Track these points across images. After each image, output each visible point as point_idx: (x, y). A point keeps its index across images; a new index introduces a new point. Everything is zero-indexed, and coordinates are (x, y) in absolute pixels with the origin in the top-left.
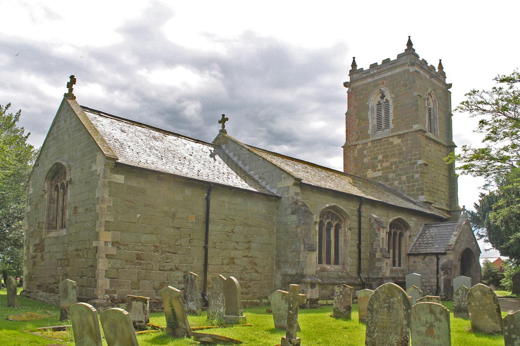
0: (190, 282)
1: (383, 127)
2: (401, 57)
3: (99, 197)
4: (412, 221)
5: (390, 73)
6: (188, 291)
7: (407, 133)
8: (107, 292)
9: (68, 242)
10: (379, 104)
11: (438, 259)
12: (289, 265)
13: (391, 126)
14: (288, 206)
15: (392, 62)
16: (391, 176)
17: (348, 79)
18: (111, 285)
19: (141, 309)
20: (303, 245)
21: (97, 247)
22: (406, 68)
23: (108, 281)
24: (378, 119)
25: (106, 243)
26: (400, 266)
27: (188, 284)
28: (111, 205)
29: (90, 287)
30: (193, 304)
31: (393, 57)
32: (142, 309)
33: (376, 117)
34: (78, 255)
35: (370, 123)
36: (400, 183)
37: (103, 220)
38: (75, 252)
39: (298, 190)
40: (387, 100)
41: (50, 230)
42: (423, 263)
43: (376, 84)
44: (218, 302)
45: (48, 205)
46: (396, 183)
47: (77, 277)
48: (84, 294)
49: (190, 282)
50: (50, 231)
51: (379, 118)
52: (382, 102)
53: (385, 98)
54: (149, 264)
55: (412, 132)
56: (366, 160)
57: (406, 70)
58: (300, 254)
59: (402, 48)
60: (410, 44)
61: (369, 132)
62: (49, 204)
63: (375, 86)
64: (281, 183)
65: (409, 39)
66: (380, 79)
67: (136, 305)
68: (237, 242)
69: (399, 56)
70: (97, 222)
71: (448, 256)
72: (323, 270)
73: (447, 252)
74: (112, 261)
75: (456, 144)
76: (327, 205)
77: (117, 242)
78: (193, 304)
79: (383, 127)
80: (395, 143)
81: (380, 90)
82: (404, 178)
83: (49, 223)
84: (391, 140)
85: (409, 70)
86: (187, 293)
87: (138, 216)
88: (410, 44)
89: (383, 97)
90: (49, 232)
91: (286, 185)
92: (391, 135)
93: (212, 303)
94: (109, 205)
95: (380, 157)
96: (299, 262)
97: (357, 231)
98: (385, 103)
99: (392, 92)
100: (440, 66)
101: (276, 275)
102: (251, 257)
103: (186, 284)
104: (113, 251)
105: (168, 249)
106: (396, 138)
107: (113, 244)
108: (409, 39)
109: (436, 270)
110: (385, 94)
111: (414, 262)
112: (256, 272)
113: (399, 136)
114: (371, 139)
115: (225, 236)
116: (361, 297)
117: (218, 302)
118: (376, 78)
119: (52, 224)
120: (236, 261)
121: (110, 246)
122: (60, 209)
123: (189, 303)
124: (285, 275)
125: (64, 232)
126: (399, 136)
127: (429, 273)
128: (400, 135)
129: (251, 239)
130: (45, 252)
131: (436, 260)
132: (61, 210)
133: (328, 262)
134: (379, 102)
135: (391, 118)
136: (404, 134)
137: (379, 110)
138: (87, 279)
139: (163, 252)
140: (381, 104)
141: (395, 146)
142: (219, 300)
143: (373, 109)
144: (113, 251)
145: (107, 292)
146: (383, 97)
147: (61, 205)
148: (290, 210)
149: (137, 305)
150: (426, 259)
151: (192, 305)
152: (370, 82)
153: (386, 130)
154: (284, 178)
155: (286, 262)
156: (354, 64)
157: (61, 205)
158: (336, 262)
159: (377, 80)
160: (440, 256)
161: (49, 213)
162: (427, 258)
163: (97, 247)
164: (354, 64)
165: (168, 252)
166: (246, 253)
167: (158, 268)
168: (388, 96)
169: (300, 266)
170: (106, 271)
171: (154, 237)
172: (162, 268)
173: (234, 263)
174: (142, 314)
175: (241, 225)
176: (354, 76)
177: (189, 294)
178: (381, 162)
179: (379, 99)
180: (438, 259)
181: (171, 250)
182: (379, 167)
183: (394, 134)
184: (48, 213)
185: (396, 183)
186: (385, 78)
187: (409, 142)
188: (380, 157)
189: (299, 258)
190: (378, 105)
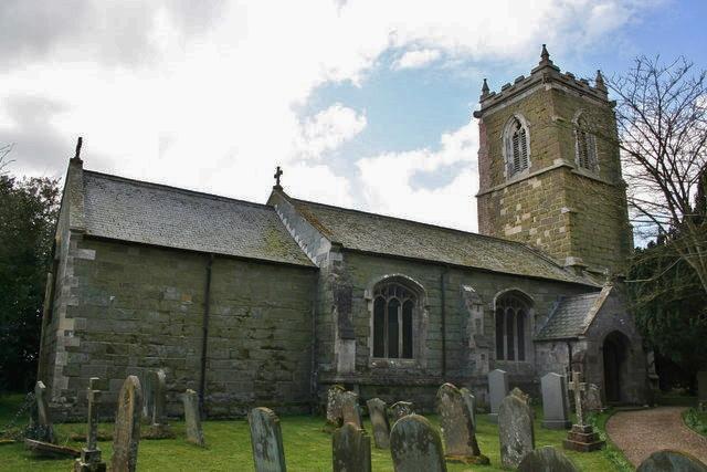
4: (538, 295)
8: (63, 394)
10: (516, 136)
13: (530, 164)
16: (533, 231)
17: (479, 107)
18: (70, 385)
22: (541, 86)
23: (66, 380)
25: (67, 333)
26: (522, 357)
28: (77, 285)
31: (527, 75)
36: (543, 241)
37: (64, 305)
39: (340, 257)
46: (539, 240)
48: (210, 387)
54: (124, 358)
56: (503, 212)
59: (536, 61)
60: (545, 54)
61: (505, 174)
68: (254, 329)
69: (534, 72)
72: (386, 366)
74: (74, 355)
76: (386, 276)
77: (82, 332)
80: (534, 187)
82: (547, 233)
84: (530, 182)
87: (112, 298)
88: (545, 54)
94: (73, 285)
95: (519, 207)
97: (439, 310)
99: (527, 119)
100: (600, 81)
102: (276, 348)
104: (75, 342)
105: (151, 339)
106: (536, 179)
107: (76, 334)
111: (543, 353)
112: (284, 368)
113: (538, 176)
114: (508, 183)
115: (236, 321)
120: (251, 354)
121: (71, 335)
126: (538, 176)
129: (276, 324)
131: (567, 349)
133: (393, 354)
135: (529, 153)
137: (516, 145)
139: (144, 343)
141: (535, 191)
144: (75, 342)
145: (63, 394)
146: (519, 126)
156: (486, 89)
158: (408, 354)
160: (572, 343)
164: (486, 89)
165: (152, 343)
166: (268, 342)
167: (136, 363)
170: (65, 367)
171: (132, 324)
172: (142, 364)
173: (248, 357)
175: (260, 306)
176: (486, 103)
178: (521, 213)
179: (515, 129)
181: (155, 340)
182: (518, 221)
185: (539, 240)
188: (519, 207)
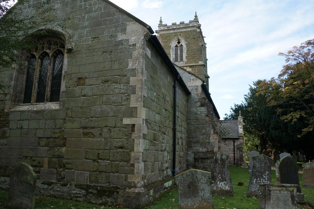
0: (219, 162)
1: (179, 60)
2: (192, 22)
3: (135, 69)
5: (185, 30)
6: (217, 171)
7: (196, 65)
9: (64, 117)
10: (176, 46)
11: (234, 143)
12: (199, 145)
14: (197, 100)
15: (185, 24)
19: (288, 200)
20: (213, 130)
21: (134, 125)
22: (195, 29)
24: (176, 55)
27: (218, 165)
29: (117, 172)
30: (225, 184)
32: (290, 199)
33: (174, 54)
34: (85, 134)
35: (172, 56)
38: (81, 130)
40: (181, 45)
41: (16, 104)
42: (224, 144)
43: (176, 34)
44: (263, 180)
45: (17, 75)
47: (85, 160)
49: (219, 162)
50: (16, 105)
51: (176, 55)
52: (178, 45)
53: (180, 44)
55: (198, 65)
57: (194, 30)
58: (210, 137)
59: (193, 18)
62: (18, 74)
63: (175, 36)
64: (190, 83)
65: (161, 19)
66: (179, 32)
67: (279, 195)
69: (190, 22)
70: (132, 96)
71: (240, 140)
73: (240, 138)
75: (209, 76)
78: (225, 184)
79: (179, 60)
81: (178, 38)
83: (16, 95)
85: (196, 30)
86: (215, 173)
88: (196, 16)
89: (179, 43)
90: (15, 105)
91: (194, 84)
92: (186, 65)
93: (254, 182)
96: (209, 143)
98: (180, 46)
101: (188, 152)
103: (214, 165)
108: (161, 19)
109: (233, 149)
110: (180, 41)
113: (190, 67)
116: (307, 169)
117: (263, 180)
118: (176, 31)
119: (20, 97)
122: (36, 81)
123: (218, 183)
124: (196, 153)
125: (54, 106)
126: (190, 67)
127: (229, 150)
128: (191, 66)
130: (10, 127)
132: (37, 82)
134: (176, 45)
136: (193, 66)
137: (176, 51)
138: (110, 163)
140: (178, 46)
142: (265, 179)
143: (173, 49)
146: (179, 43)
147: (37, 76)
148: (199, 104)
149: (281, 195)
150: (226, 142)
151: (223, 185)
152: (172, 33)
153: (180, 62)
154: (193, 80)
155: (197, 142)
156: (161, 21)
157: (37, 76)
159: (176, 32)
161: (16, 83)
162: (227, 141)
163: (134, 125)
164: (161, 21)
168: (183, 43)
169: (210, 145)
174: (289, 206)
177: (219, 174)
180: (234, 143)
183: (187, 65)
184: (15, 84)
186: (181, 32)
187: (196, 71)
189: (209, 140)
190: (175, 47)
